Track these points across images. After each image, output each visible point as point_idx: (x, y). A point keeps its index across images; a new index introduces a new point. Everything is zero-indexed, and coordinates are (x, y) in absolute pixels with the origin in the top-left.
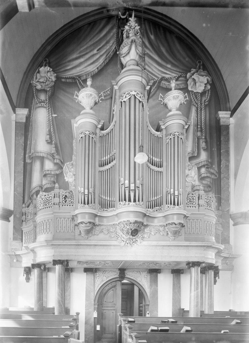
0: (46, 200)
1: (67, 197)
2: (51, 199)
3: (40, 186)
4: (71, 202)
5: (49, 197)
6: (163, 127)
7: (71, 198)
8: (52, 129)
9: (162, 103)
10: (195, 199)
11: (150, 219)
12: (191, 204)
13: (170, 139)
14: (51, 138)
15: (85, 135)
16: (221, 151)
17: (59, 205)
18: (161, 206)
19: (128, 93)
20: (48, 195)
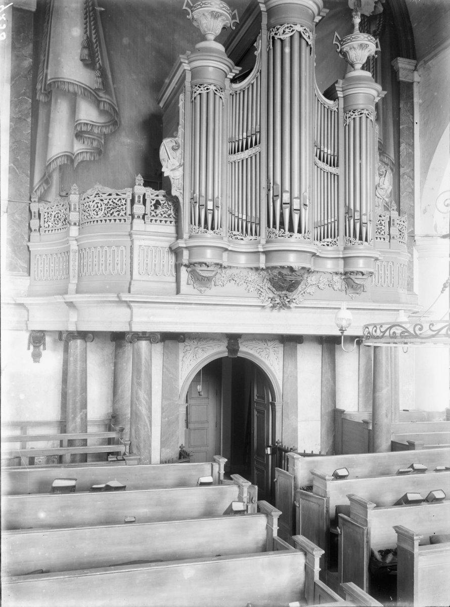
0: (111, 203)
1: (161, 205)
2: (125, 204)
3: (67, 156)
4: (169, 216)
5: (120, 199)
6: (340, 94)
7: (168, 207)
8: (94, 36)
9: (339, 50)
10: (383, 224)
11: (320, 260)
12: (378, 233)
13: (354, 118)
14: (92, 55)
15: (208, 91)
16: (401, 127)
17: (144, 218)
18: (335, 237)
19: (289, 25)
20: (117, 195)
